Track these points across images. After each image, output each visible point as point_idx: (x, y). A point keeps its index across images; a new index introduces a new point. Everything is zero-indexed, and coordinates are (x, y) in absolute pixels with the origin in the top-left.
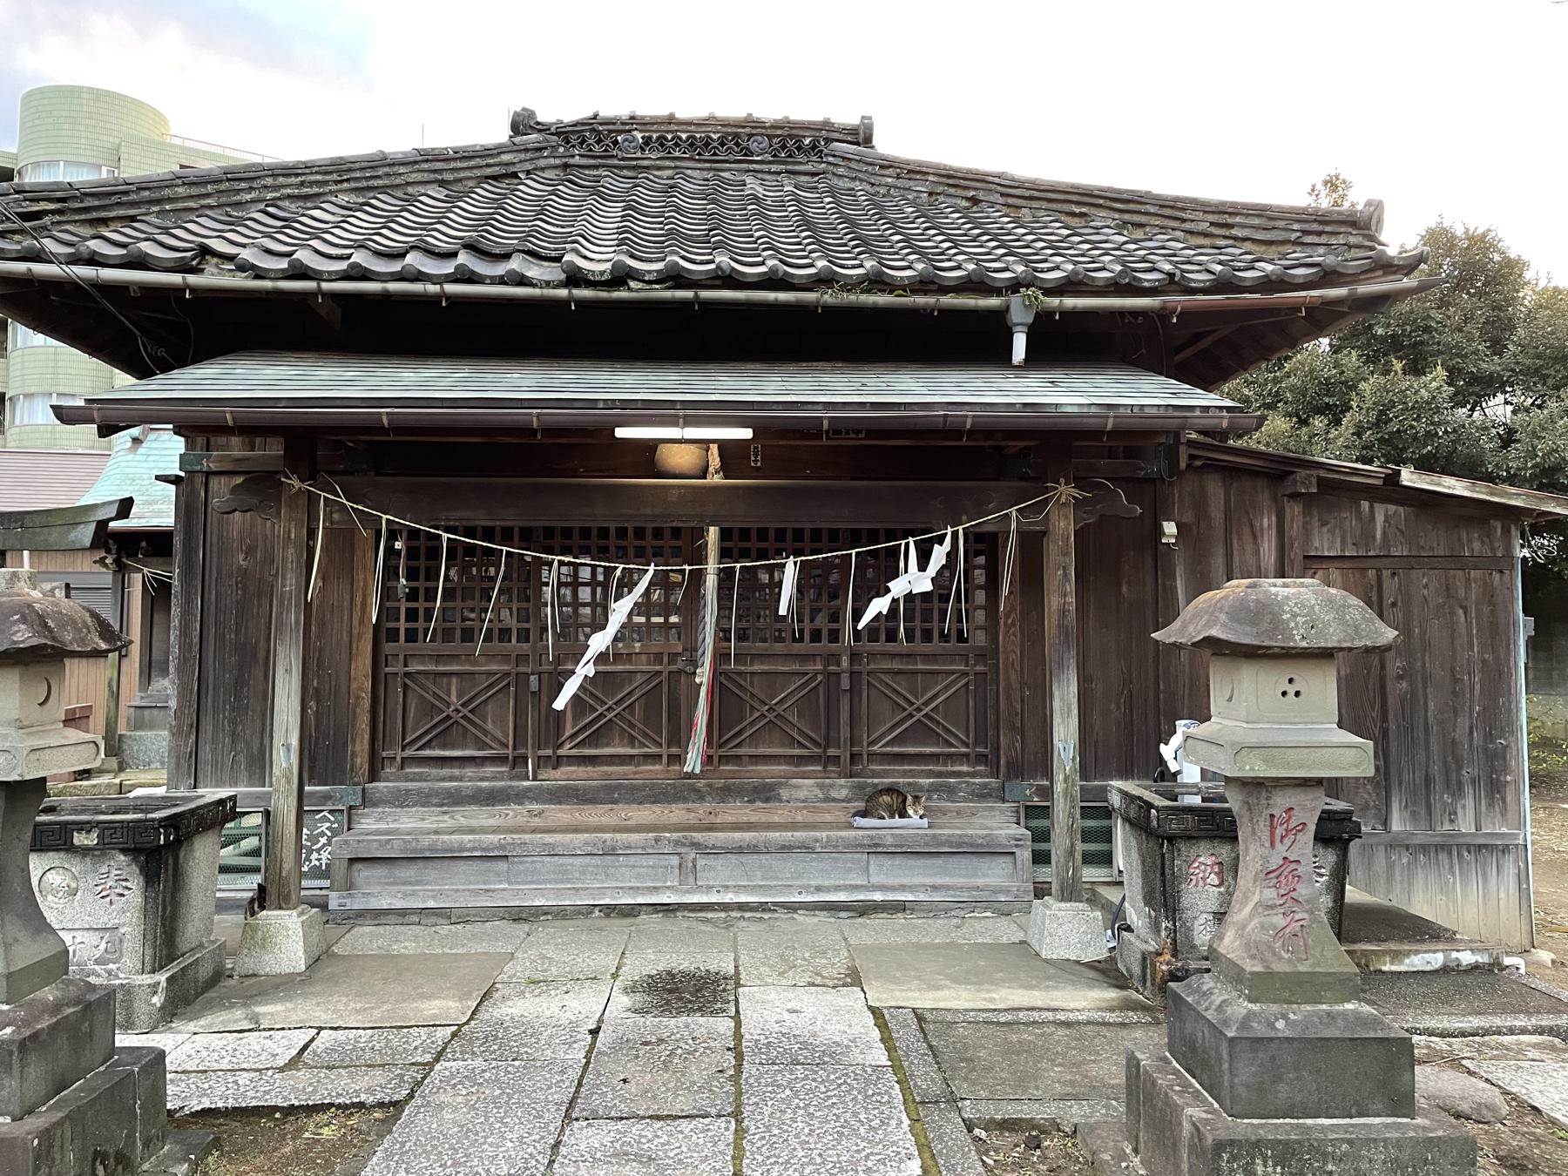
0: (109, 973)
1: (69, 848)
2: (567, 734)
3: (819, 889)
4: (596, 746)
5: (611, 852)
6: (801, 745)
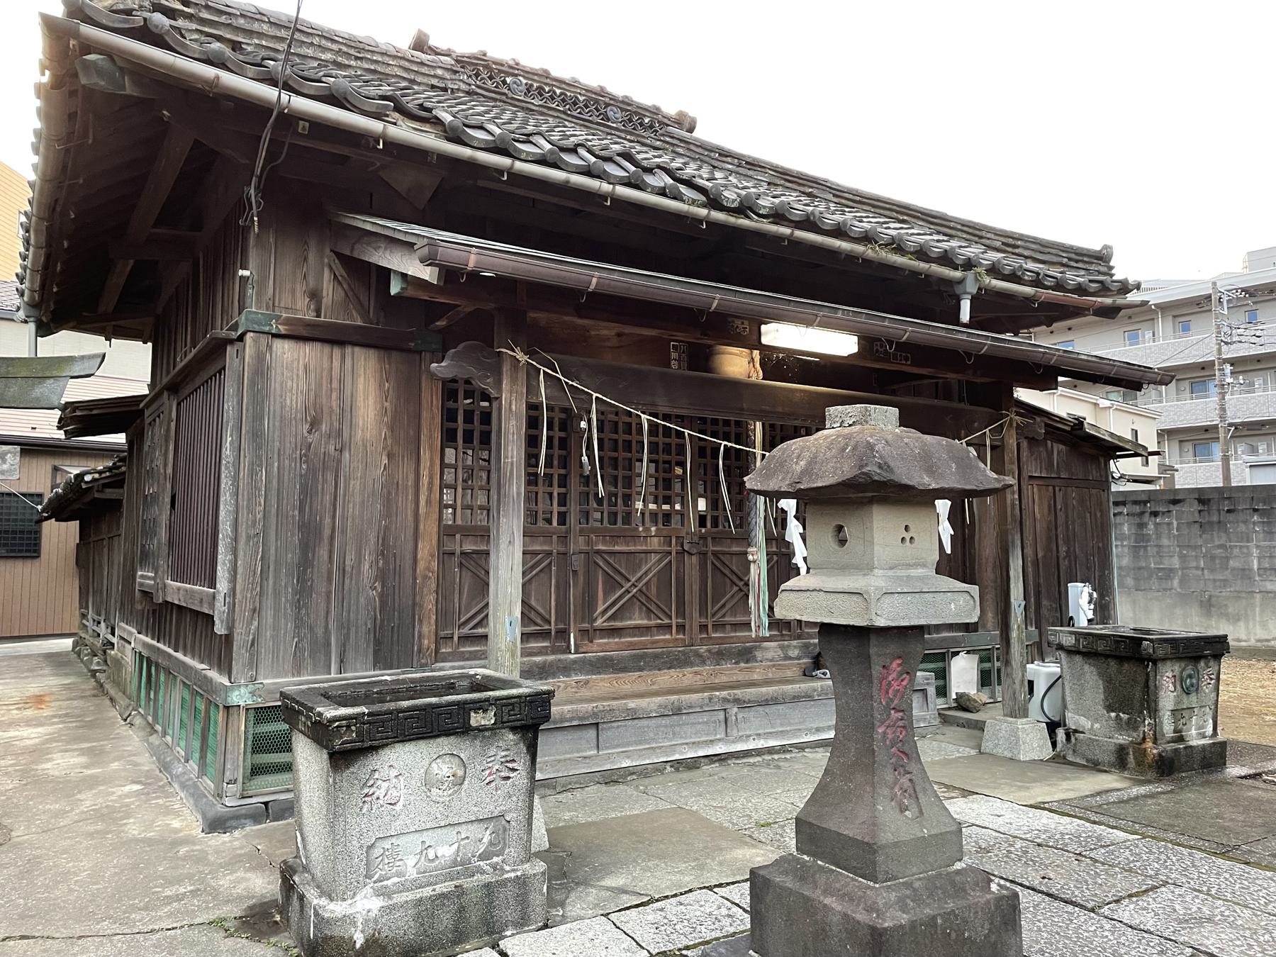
0: (494, 867)
2: (601, 608)
3: (818, 730)
4: (622, 620)
5: (677, 712)
6: (537, 624)
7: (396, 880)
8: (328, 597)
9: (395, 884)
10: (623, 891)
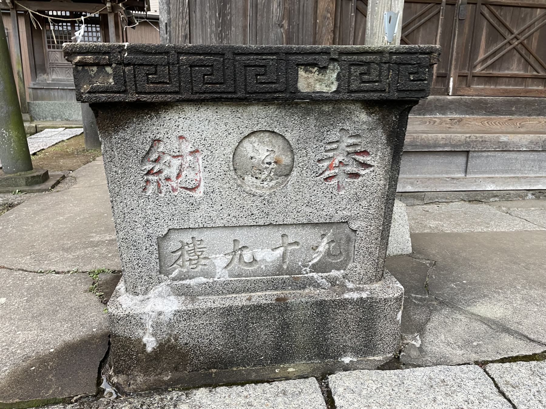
0: (333, 282)
1: (287, 98)
2: (481, 56)
4: (500, 70)
7: (203, 280)
8: (244, 30)
9: (200, 285)
10: (501, 327)
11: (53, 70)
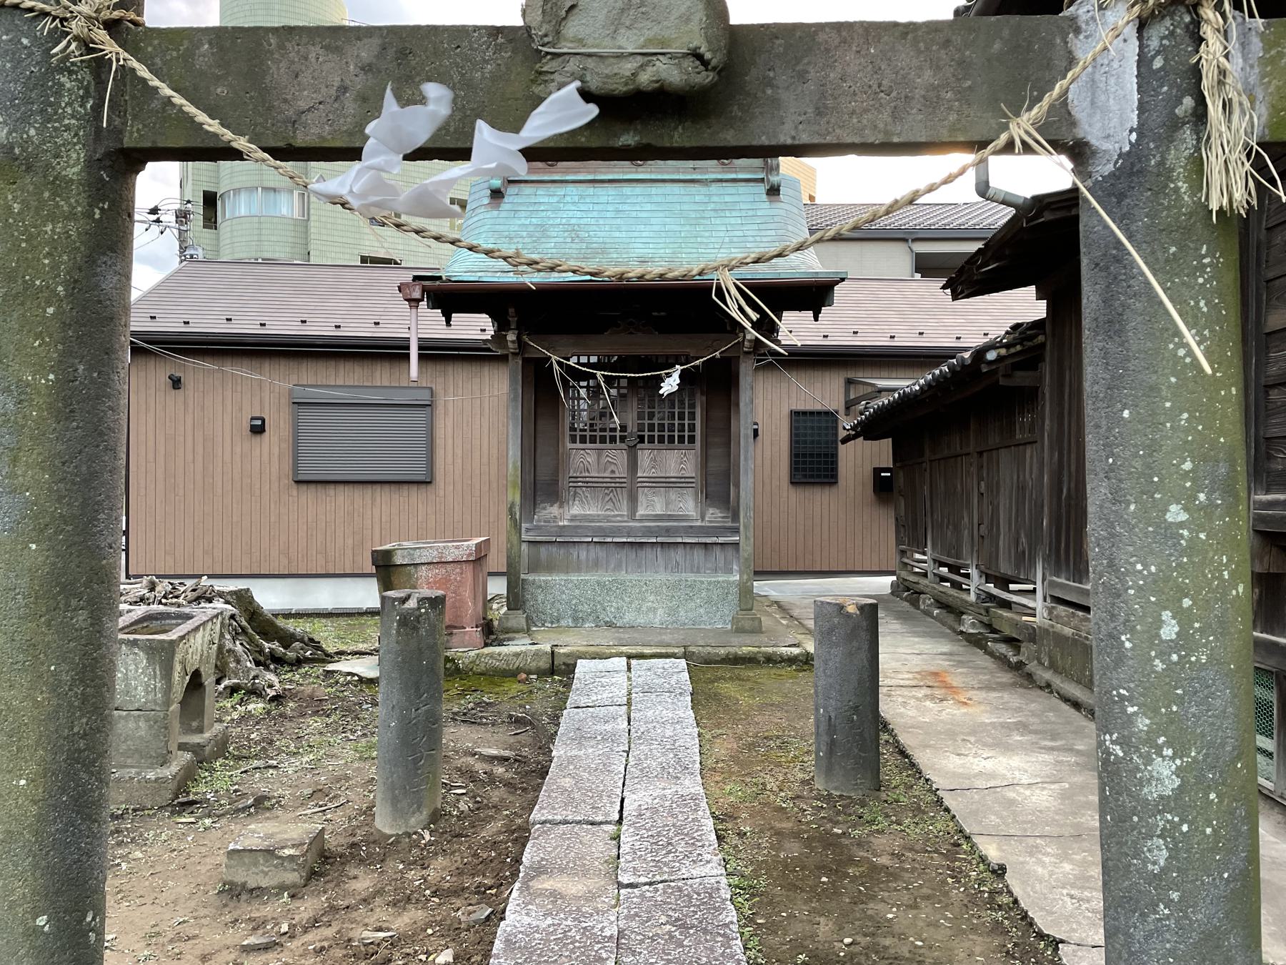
11: (575, 493)
